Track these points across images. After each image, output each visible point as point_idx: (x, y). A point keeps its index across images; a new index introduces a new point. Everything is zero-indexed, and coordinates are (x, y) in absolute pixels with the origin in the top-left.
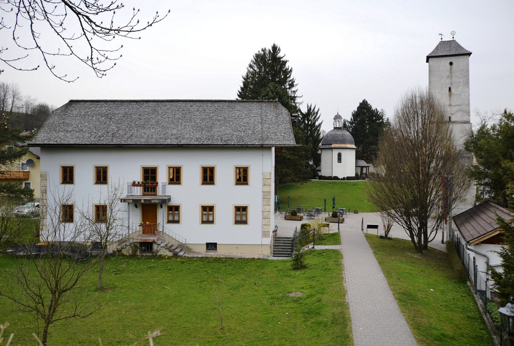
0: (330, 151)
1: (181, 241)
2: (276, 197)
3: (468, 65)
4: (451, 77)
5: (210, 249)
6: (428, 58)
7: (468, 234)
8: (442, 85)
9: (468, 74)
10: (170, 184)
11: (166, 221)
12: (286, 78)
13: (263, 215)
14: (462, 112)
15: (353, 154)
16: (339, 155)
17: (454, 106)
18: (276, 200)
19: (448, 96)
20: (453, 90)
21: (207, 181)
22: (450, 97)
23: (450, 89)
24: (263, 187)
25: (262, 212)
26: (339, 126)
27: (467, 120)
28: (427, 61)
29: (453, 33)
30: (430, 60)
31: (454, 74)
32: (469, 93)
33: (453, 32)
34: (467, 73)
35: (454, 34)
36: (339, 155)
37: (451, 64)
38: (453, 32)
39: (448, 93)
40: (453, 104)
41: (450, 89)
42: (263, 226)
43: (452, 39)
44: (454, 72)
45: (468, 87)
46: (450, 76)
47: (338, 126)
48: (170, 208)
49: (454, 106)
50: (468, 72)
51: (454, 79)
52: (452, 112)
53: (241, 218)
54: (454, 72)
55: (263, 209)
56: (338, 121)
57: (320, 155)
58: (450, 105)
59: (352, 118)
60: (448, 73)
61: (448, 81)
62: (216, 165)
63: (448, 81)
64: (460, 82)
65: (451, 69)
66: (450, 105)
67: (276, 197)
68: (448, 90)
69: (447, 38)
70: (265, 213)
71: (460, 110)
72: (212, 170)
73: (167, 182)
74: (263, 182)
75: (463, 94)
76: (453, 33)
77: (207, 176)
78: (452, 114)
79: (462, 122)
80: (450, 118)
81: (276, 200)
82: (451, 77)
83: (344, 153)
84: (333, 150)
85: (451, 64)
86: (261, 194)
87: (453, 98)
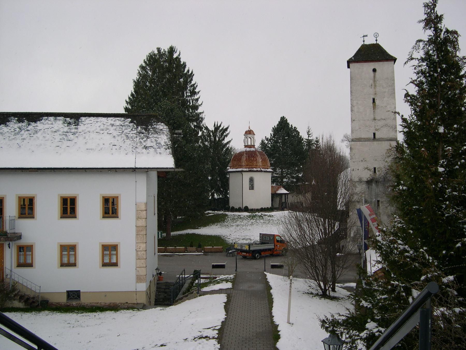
0: (239, 174)
1: (33, 289)
2: (160, 233)
3: (393, 72)
4: (375, 86)
5: (71, 299)
6: (349, 62)
7: (379, 272)
8: (365, 95)
9: (394, 84)
10: (20, 217)
11: (14, 263)
12: (186, 83)
13: (137, 255)
14: (387, 127)
15: (268, 177)
16: (251, 180)
17: (379, 120)
18: (160, 237)
19: (372, 109)
20: (377, 102)
21: (67, 213)
22: (373, 109)
23: (374, 100)
24: (136, 220)
25: (135, 251)
26: (251, 144)
27: (394, 137)
28: (349, 67)
29: (376, 36)
30: (351, 65)
31: (378, 82)
32: (395, 105)
33: (376, 34)
34: (392, 82)
35: (377, 36)
36: (251, 180)
37: (374, 70)
38: (376, 34)
39: (372, 105)
40: (378, 117)
41: (374, 100)
42: (137, 269)
43: (375, 42)
44: (378, 80)
45: (394, 98)
46: (373, 85)
47: (249, 144)
48: (21, 249)
49: (379, 120)
50: (394, 80)
51: (378, 89)
52: (377, 127)
53: (110, 259)
54: (378, 80)
55: (137, 247)
56: (250, 138)
57: (228, 179)
58: (374, 119)
59: (272, 135)
60: (371, 82)
61: (371, 91)
62: (120, 195)
63: (371, 91)
64: (385, 92)
65: (374, 77)
66: (374, 119)
67: (160, 233)
68: (372, 101)
69: (370, 41)
70: (139, 253)
71: (386, 125)
72: (31, 201)
73: (17, 216)
74: (137, 214)
75: (388, 107)
76: (376, 36)
77: (67, 207)
78: (376, 130)
79: (388, 139)
80: (374, 134)
81: (160, 237)
82: (375, 86)
83: (257, 177)
84: (243, 173)
85: (374, 70)
86: (134, 229)
87: (377, 111)
